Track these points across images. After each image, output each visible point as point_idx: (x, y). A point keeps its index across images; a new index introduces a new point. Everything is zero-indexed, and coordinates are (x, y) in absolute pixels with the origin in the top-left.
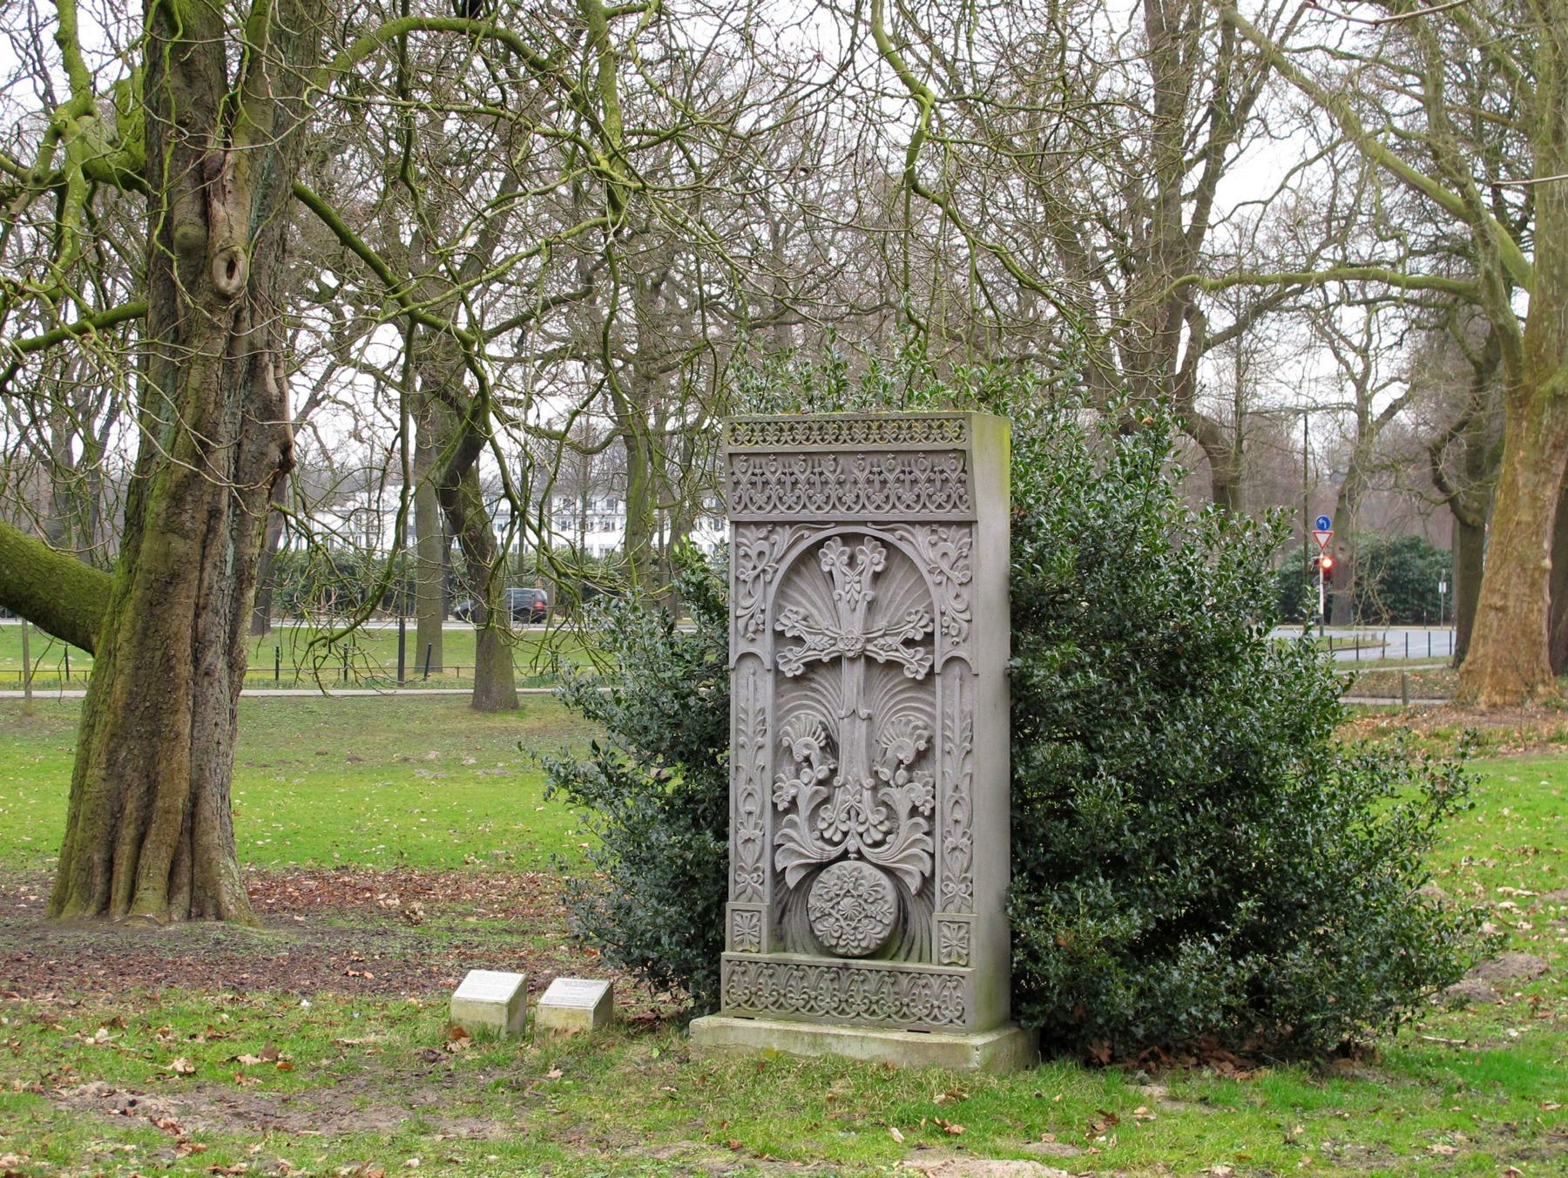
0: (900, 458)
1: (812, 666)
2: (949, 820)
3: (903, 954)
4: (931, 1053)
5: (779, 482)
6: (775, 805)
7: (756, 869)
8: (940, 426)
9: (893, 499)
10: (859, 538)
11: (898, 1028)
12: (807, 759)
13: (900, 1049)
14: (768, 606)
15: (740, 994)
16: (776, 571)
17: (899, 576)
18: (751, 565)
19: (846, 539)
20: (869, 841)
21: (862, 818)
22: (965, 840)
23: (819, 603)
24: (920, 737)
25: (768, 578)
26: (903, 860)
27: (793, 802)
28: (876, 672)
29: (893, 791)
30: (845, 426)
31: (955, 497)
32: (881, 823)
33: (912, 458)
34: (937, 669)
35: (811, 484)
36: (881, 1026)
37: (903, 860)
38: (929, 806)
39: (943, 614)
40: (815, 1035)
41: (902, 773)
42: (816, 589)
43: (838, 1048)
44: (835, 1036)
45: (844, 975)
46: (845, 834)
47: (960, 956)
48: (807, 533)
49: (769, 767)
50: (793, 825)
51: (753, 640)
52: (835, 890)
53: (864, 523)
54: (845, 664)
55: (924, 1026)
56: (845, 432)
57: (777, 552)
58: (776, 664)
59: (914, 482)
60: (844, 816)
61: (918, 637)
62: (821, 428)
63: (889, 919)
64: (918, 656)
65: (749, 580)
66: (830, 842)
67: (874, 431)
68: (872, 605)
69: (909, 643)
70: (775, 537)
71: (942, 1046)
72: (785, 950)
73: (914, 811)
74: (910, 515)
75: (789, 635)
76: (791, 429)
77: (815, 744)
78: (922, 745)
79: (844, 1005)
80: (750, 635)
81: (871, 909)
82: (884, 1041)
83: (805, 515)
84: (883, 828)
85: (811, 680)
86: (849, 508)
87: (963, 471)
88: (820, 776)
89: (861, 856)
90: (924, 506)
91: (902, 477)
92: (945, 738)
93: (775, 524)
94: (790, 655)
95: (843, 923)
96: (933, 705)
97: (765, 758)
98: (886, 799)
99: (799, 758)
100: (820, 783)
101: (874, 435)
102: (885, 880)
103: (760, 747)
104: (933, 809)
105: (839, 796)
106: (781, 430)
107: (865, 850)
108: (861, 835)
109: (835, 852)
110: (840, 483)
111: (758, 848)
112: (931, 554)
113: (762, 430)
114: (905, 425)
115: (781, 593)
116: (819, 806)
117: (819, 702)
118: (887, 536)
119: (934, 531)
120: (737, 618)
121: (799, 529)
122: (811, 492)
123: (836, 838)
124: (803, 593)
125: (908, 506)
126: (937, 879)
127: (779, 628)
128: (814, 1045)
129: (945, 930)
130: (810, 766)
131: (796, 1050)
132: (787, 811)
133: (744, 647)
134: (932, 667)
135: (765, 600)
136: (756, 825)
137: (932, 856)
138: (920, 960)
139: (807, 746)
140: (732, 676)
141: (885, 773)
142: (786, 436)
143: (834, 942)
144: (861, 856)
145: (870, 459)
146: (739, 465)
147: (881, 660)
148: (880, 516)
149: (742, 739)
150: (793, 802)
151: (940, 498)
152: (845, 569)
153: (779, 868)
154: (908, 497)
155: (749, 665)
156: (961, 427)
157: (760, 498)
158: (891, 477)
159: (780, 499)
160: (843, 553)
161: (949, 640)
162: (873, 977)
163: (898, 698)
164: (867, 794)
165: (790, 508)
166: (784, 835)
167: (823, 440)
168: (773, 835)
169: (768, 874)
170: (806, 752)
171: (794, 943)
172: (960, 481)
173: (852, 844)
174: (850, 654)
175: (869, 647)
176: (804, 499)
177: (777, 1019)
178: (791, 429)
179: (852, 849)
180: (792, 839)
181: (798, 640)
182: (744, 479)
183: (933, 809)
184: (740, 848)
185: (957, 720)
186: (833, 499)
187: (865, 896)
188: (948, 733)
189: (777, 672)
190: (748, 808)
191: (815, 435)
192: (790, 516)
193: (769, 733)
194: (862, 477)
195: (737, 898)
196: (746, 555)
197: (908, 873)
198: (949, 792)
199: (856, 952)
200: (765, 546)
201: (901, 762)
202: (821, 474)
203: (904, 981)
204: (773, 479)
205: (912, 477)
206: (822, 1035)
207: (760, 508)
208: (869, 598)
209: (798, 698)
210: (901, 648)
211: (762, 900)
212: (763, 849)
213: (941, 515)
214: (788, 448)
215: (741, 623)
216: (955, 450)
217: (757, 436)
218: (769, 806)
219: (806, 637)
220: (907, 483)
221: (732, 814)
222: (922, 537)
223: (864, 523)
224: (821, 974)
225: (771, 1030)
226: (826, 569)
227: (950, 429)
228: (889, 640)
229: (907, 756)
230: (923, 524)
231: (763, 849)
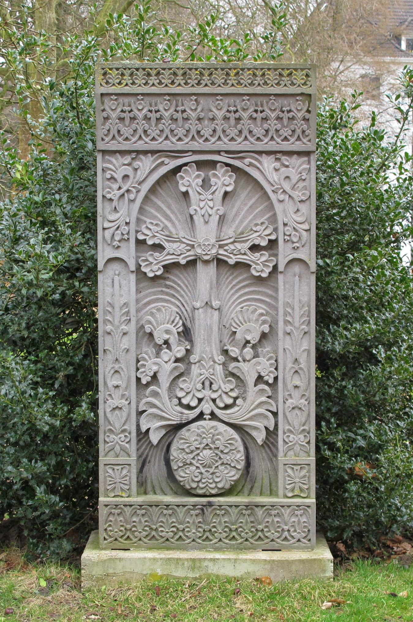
2: (290, 386)
3: (246, 490)
4: (294, 568)
5: (146, 118)
6: (138, 380)
7: (124, 431)
8: (290, 74)
9: (245, 132)
10: (213, 164)
11: (253, 548)
12: (166, 342)
13: (268, 567)
15: (116, 531)
16: (138, 191)
18: (115, 186)
19: (200, 165)
20: (222, 405)
21: (215, 387)
22: (303, 401)
24: (264, 322)
25: (132, 196)
27: (155, 377)
28: (224, 270)
29: (241, 364)
30: (206, 73)
32: (232, 390)
34: (281, 268)
36: (240, 548)
38: (272, 376)
39: (285, 225)
40: (193, 560)
42: (174, 206)
43: (213, 569)
44: (211, 560)
45: (208, 511)
46: (200, 400)
47: (301, 490)
48: (167, 160)
49: (133, 349)
50: (155, 394)
51: (119, 247)
53: (218, 152)
54: (199, 265)
55: (276, 546)
56: (206, 78)
57: (140, 175)
58: (139, 266)
60: (199, 386)
61: (264, 243)
62: (184, 74)
64: (263, 259)
65: (115, 198)
66: (189, 407)
67: (232, 77)
68: (222, 219)
69: (254, 248)
70: (136, 164)
71: (302, 561)
72: (145, 493)
73: (260, 379)
74: (259, 147)
75: (150, 242)
76: (158, 74)
77: (175, 331)
78: (266, 328)
80: (116, 243)
81: (226, 458)
82: (253, 561)
83: (167, 145)
86: (207, 140)
87: (308, 111)
88: (179, 355)
89: (213, 416)
91: (255, 115)
92: (286, 322)
93: (138, 152)
94: (151, 259)
95: (203, 470)
97: (129, 342)
98: (235, 371)
99: (161, 342)
101: (232, 80)
102: (236, 436)
103: (124, 334)
104: (276, 379)
105: (195, 370)
106: (149, 75)
107: (218, 412)
108: (214, 401)
109: (193, 414)
110: (199, 119)
111: (125, 415)
113: (131, 75)
114: (259, 73)
115: (141, 210)
116: (178, 377)
117: (174, 296)
119: (277, 159)
120: (104, 229)
121: (160, 157)
123: (194, 403)
124: (159, 209)
125: (258, 139)
126: (280, 432)
127: (141, 237)
128: (193, 568)
129: (289, 471)
130: (169, 347)
131: (180, 573)
134: (275, 267)
135: (129, 215)
136: (123, 396)
138: (261, 494)
139: (167, 332)
141: (234, 351)
142: (153, 80)
143: (194, 485)
145: (227, 100)
146: (109, 104)
147: (231, 262)
148: (233, 147)
149: (109, 328)
150: (155, 377)
151: (286, 132)
152: (199, 189)
153: (144, 429)
154: (259, 131)
156: (307, 76)
157: (259, 131)
159: (224, 131)
160: (198, 176)
161: (290, 245)
162: (234, 511)
163: (242, 292)
167: (107, 83)
168: (138, 403)
169: (134, 434)
170: (166, 336)
171: (153, 487)
172: (304, 119)
173: (207, 407)
174: (206, 258)
175: (221, 252)
176: (167, 131)
177: (150, 548)
178: (158, 74)
179: (207, 411)
181: (159, 247)
182: (114, 115)
183: (276, 379)
184: (109, 415)
185: (297, 308)
186: (193, 132)
187: (222, 448)
188: (288, 318)
190: (116, 383)
191: (179, 79)
192: (154, 145)
193: (133, 322)
194: (220, 114)
196: (112, 178)
197: (255, 428)
198: (290, 365)
199: (213, 492)
200: (129, 171)
201: (248, 342)
202: (184, 111)
203: (260, 512)
204: (141, 115)
205: (263, 115)
206: (200, 560)
207: (127, 139)
208: (221, 213)
209: (154, 293)
210: (248, 252)
212: (129, 415)
213: (286, 146)
214: (154, 90)
215: (108, 234)
216: (302, 94)
218: (134, 380)
219: (166, 245)
222: (268, 163)
223: (218, 152)
225: (154, 559)
226: (184, 189)
227: (299, 77)
229: (254, 337)
230: (269, 153)
231: (129, 415)
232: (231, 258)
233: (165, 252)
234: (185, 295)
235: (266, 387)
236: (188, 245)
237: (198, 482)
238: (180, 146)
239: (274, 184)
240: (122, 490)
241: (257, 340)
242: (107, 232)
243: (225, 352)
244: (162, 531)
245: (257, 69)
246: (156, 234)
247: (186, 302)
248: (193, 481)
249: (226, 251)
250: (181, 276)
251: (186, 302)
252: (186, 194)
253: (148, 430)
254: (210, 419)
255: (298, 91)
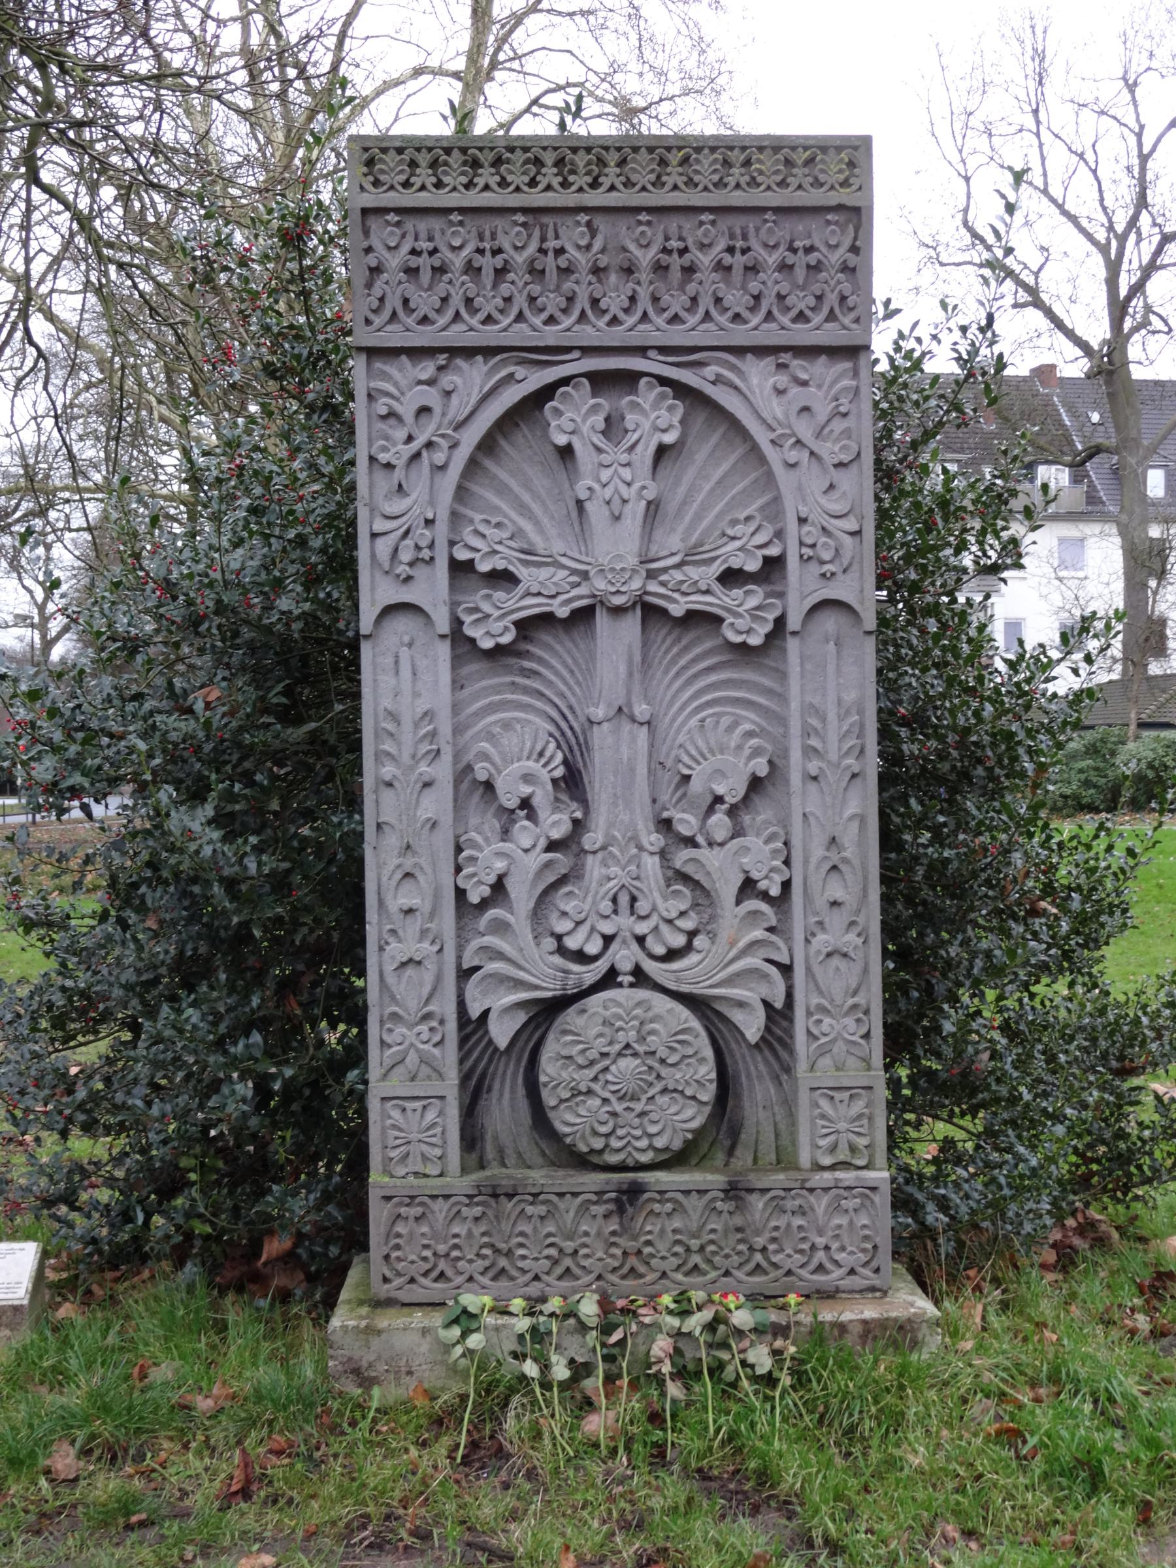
0: (725, 222)
1: (526, 627)
2: (821, 903)
6: (460, 893)
7: (427, 1017)
9: (706, 302)
14: (443, 516)
16: (454, 446)
17: (700, 457)
18: (401, 434)
19: (600, 381)
20: (660, 950)
21: (643, 907)
22: (851, 937)
23: (536, 508)
24: (757, 752)
25: (439, 457)
26: (728, 982)
27: (499, 887)
28: (661, 634)
31: (832, 299)
32: (682, 914)
33: (751, 222)
34: (793, 623)
35: (536, 273)
37: (728, 982)
38: (778, 879)
39: (802, 521)
41: (719, 822)
46: (608, 940)
47: (853, 1149)
48: (520, 371)
49: (447, 819)
50: (500, 927)
51: (408, 579)
52: (600, 1045)
53: (641, 351)
54: (602, 619)
57: (458, 407)
58: (457, 623)
59: (752, 269)
60: (606, 906)
61: (753, 566)
63: (708, 1094)
64: (752, 602)
65: (400, 463)
66: (581, 957)
68: (653, 508)
69: (731, 577)
73: (748, 887)
74: (740, 335)
75: (484, 567)
76: (498, 162)
77: (545, 776)
78: (761, 767)
79: (633, 1261)
80: (402, 569)
81: (674, 1077)
83: (521, 335)
84: (688, 924)
85: (526, 655)
86: (614, 321)
87: (854, 249)
88: (556, 835)
89: (640, 977)
90: (769, 316)
92: (810, 752)
93: (454, 352)
94: (486, 607)
95: (619, 1107)
96: (782, 698)
98: (689, 869)
99: (512, 803)
100: (552, 846)
101: (674, 175)
104: (786, 885)
105: (593, 867)
108: (641, 940)
109: (590, 974)
111: (428, 978)
112: (775, 409)
113: (434, 164)
115: (461, 493)
118: (686, 377)
119: (782, 366)
120: (374, 536)
122: (536, 289)
127: (462, 555)
129: (825, 1104)
130: (532, 816)
132: (484, 904)
133: (390, 593)
134: (780, 622)
135: (432, 502)
136: (424, 933)
137: (786, 970)
139: (527, 778)
140: (366, 649)
141: (686, 822)
142: (487, 176)
143: (598, 1144)
144: (640, 977)
147: (677, 610)
148: (677, 336)
150: (499, 887)
152: (598, 440)
153: (475, 1011)
155: (402, 625)
158: (705, 260)
160: (595, 409)
161: (814, 569)
164: (652, 863)
165: (489, 320)
166: (483, 948)
169: (452, 1025)
170: (526, 790)
173: (624, 956)
174: (618, 601)
175: (653, 587)
176: (520, 302)
179: (625, 966)
180: (501, 956)
181: (503, 578)
182: (394, 262)
184: (391, 979)
185: (832, 716)
187: (662, 1052)
189: (457, 637)
190: (405, 902)
192: (490, 336)
193: (447, 757)
195: (385, 1076)
196: (391, 414)
197: (741, 1004)
198: (818, 852)
199: (645, 1158)
200: (430, 396)
201: (718, 799)
209: (496, 689)
210: (717, 587)
211: (441, 1076)
213: (803, 335)
215: (383, 547)
216: (840, 208)
217: (424, 175)
220: (738, 271)
221: (371, 915)
223: (641, 351)
224: (585, 1206)
228: (693, 572)
229: (732, 788)
231: (439, 979)
232: (675, 601)
233: (520, 589)
234: (568, 694)
235: (764, 907)
236: (574, 572)
237: (607, 1135)
238: (551, 336)
239: (774, 425)
240: (425, 1158)
241: (741, 793)
242: (380, 542)
243: (665, 825)
244: (524, 1257)
245: (731, 148)
246: (498, 547)
247: (571, 708)
248: (595, 1133)
249: (663, 584)
250: (558, 647)
251: (571, 708)
252: (566, 452)
253: (485, 1014)
254: (632, 985)
255: (833, 199)
